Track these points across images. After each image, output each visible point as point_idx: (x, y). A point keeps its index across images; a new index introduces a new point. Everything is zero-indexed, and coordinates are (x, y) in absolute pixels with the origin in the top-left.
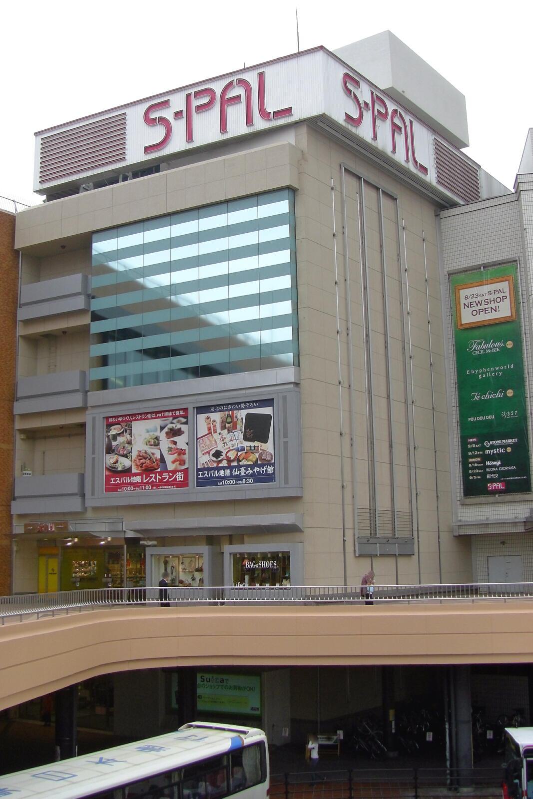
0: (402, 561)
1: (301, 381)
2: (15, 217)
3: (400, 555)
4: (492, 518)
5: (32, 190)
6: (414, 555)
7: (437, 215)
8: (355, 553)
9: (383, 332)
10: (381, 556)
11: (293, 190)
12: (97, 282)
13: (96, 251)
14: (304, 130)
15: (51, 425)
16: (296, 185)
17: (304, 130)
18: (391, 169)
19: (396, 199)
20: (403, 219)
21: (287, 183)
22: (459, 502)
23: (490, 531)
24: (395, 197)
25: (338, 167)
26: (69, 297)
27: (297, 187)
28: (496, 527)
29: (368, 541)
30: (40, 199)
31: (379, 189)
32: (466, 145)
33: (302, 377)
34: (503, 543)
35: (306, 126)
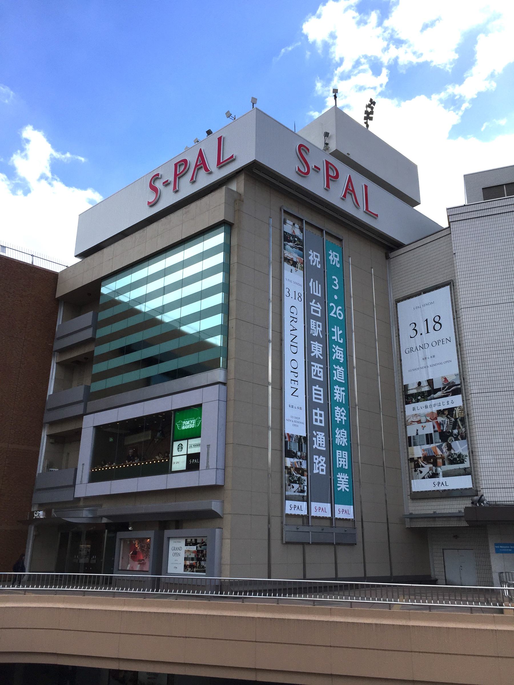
0: (342, 551)
1: (228, 381)
2: (58, 275)
3: (338, 544)
4: (438, 512)
5: (74, 255)
6: (356, 544)
7: (387, 257)
8: (282, 540)
9: (279, 331)
10: (313, 543)
11: (230, 225)
12: (103, 315)
13: (148, 307)
14: (242, 178)
15: (66, 430)
16: (231, 220)
17: (242, 178)
18: (306, 199)
19: (341, 240)
20: (349, 257)
21: (221, 218)
22: (409, 496)
23: (439, 524)
24: (341, 238)
25: (279, 210)
26: (86, 329)
27: (232, 222)
28: (448, 521)
29: (323, 530)
30: (78, 260)
31: (323, 230)
32: (417, 203)
33: (229, 378)
34: (456, 537)
35: (243, 174)
